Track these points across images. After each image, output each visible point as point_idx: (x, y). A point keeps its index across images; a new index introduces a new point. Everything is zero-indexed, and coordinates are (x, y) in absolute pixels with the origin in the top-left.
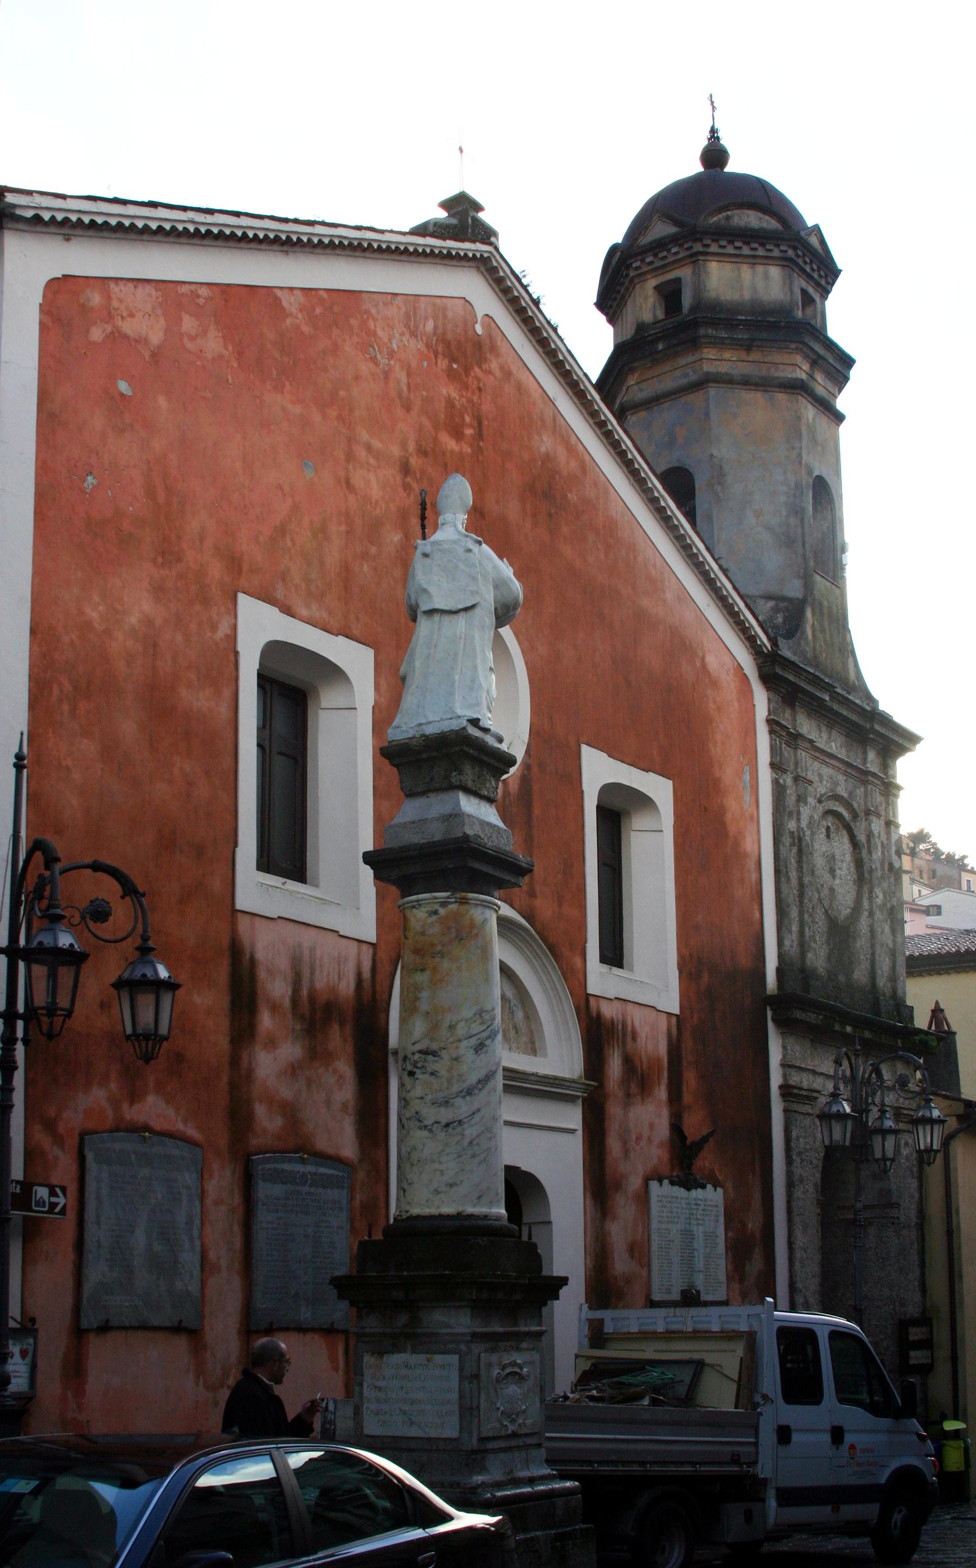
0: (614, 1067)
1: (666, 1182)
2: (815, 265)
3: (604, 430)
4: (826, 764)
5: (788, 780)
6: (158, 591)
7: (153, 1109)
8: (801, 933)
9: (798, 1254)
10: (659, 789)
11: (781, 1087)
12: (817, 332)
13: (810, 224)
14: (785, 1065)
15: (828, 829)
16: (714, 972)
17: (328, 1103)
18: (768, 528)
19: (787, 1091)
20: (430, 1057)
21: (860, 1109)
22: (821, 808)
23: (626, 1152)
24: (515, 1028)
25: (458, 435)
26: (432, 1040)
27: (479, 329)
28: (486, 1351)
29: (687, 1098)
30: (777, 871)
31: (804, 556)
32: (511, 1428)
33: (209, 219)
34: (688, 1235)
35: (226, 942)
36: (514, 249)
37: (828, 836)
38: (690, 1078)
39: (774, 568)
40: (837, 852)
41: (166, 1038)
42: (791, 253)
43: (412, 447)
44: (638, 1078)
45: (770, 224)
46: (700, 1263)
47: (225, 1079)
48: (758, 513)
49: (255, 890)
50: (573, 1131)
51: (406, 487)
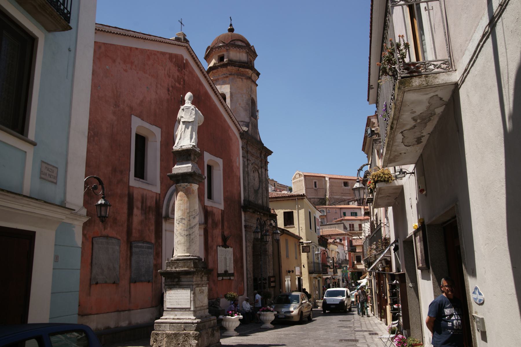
0: (210, 221)
2: (252, 53)
3: (327, 203)
5: (246, 160)
6: (114, 113)
7: (109, 231)
8: (248, 193)
9: (248, 262)
10: (220, 161)
12: (252, 68)
13: (251, 45)
14: (245, 221)
16: (230, 199)
17: (149, 230)
18: (242, 107)
19: (246, 226)
23: (213, 241)
25: (180, 84)
27: (185, 61)
29: (225, 227)
30: (244, 179)
33: (128, 32)
34: (226, 259)
35: (127, 192)
36: (193, 44)
38: (226, 224)
41: (348, 260)
43: (170, 85)
44: (215, 225)
45: (244, 44)
46: (228, 265)
47: (126, 224)
48: (240, 104)
49: (133, 182)
51: (168, 94)
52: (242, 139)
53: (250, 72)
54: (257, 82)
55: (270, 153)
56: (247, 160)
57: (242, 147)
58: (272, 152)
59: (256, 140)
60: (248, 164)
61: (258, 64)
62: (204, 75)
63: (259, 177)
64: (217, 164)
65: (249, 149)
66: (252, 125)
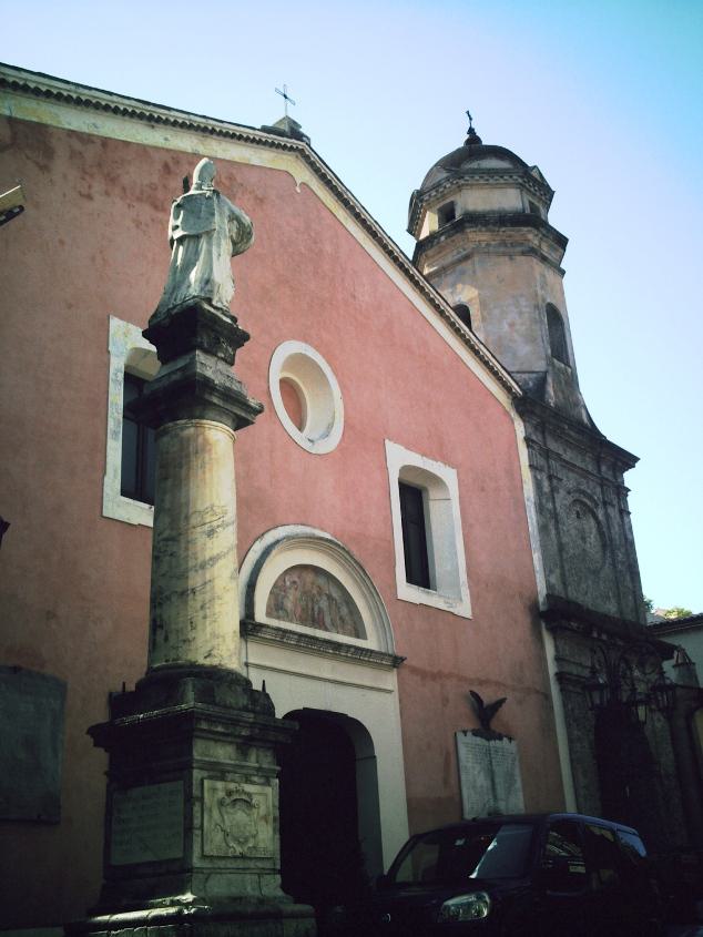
1: (469, 734)
2: (540, 190)
4: (573, 471)
11: (556, 674)
14: (558, 659)
15: (578, 513)
20: (170, 543)
21: (614, 686)
22: (570, 499)
24: (341, 618)
26: (172, 529)
28: (210, 778)
31: (544, 347)
32: (239, 850)
37: (578, 517)
39: (529, 355)
40: (586, 527)
42: (520, 181)
50: (390, 692)
52: (521, 414)
53: (532, 237)
54: (563, 266)
55: (628, 460)
56: (550, 478)
57: (527, 440)
58: (636, 459)
59: (580, 422)
60: (553, 490)
61: (556, 217)
62: (406, 272)
63: (601, 533)
64: (436, 480)
65: (553, 445)
66: (557, 381)
